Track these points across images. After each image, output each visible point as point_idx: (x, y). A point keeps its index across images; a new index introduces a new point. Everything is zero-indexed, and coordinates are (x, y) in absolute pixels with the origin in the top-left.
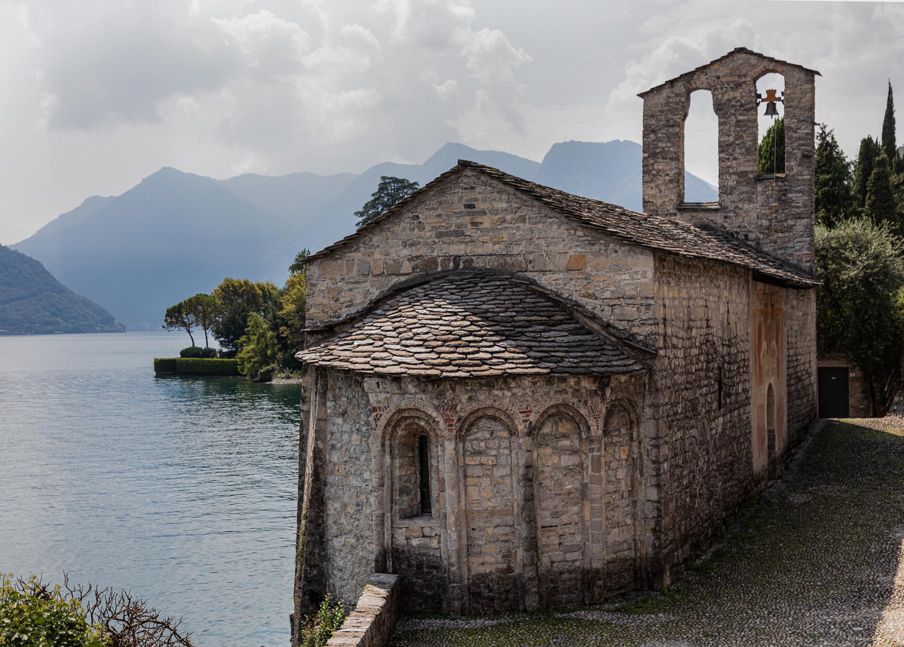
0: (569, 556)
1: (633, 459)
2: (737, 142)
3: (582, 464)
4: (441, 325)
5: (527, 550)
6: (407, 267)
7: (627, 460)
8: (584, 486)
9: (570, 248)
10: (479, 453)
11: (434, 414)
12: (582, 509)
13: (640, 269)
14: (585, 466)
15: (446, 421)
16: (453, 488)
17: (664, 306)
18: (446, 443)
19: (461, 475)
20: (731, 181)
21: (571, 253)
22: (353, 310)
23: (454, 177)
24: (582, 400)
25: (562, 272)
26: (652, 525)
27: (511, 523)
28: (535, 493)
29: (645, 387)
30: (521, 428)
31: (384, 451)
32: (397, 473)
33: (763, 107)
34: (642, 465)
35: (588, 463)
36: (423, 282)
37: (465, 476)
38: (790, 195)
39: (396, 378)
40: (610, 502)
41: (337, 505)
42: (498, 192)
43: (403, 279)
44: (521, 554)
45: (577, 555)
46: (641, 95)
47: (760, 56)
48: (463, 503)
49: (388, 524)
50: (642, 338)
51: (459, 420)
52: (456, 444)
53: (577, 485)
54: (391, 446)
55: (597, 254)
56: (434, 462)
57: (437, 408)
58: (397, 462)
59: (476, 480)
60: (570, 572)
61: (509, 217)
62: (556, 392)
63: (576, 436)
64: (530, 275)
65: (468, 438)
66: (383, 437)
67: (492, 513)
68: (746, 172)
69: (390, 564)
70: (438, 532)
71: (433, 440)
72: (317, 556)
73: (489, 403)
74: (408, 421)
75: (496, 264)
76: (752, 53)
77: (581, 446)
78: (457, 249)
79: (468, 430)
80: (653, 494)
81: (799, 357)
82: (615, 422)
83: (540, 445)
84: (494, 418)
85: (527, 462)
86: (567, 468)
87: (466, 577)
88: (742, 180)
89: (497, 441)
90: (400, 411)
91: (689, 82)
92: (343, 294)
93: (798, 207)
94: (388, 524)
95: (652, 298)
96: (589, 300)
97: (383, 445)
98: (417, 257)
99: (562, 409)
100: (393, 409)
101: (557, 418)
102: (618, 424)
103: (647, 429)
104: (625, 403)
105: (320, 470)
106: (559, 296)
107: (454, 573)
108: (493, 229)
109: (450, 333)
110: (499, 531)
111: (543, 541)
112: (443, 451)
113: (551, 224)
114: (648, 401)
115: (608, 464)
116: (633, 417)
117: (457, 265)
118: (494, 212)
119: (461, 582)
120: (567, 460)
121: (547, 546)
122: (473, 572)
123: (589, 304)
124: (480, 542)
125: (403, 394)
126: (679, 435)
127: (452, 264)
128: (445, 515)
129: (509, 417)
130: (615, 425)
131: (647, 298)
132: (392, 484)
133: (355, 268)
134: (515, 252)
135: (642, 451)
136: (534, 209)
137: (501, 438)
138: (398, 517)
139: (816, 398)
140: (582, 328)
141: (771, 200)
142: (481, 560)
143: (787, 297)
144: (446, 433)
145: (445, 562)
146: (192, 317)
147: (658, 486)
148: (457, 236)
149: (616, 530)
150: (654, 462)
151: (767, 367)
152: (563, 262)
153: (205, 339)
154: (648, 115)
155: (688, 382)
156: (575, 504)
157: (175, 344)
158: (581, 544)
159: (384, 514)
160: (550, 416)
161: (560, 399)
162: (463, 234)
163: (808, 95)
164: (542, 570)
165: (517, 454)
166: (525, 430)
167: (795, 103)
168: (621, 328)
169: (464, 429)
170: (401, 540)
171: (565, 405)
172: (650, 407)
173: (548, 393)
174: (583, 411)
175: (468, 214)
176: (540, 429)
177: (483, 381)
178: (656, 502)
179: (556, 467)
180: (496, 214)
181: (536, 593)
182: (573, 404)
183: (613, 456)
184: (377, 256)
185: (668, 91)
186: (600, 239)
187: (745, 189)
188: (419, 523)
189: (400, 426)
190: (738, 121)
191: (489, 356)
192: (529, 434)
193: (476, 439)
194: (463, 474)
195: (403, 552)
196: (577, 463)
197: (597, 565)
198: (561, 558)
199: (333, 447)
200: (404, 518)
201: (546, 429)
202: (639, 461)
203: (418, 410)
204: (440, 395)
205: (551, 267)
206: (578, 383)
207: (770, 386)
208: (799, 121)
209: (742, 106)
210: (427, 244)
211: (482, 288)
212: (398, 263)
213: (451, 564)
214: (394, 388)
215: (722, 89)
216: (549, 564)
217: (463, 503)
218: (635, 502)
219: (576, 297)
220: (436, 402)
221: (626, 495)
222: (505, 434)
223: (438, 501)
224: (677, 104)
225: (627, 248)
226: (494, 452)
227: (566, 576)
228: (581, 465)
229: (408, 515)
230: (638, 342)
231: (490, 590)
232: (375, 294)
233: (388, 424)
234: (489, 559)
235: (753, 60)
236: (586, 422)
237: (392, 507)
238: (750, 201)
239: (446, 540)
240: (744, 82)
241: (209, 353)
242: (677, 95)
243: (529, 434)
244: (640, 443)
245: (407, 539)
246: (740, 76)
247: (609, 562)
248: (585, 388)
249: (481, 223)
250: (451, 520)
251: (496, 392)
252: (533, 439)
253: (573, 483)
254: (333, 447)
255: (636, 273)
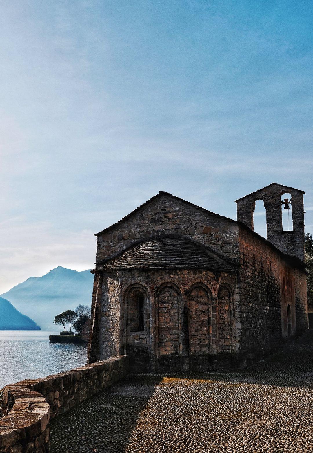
0: (203, 349)
1: (230, 310)
2: (274, 219)
3: (209, 309)
4: (150, 252)
5: (184, 345)
6: (138, 235)
7: (228, 311)
8: (209, 319)
9: (204, 225)
10: (165, 302)
11: (146, 285)
12: (208, 329)
13: (233, 231)
14: (210, 310)
15: (150, 288)
16: (153, 317)
17: (244, 248)
18: (150, 298)
19: (157, 311)
20: (272, 234)
21: (205, 226)
22: (115, 254)
23: (158, 198)
24: (209, 282)
25: (201, 234)
26: (239, 339)
27: (178, 333)
28: (188, 319)
29: (235, 280)
30: (182, 291)
31: (124, 302)
32: (130, 312)
33: (283, 206)
34: (234, 313)
35: (211, 309)
36: (146, 239)
37: (159, 312)
38: (295, 239)
39: (130, 270)
40: (220, 327)
41: (105, 329)
42: (175, 204)
43: (136, 241)
44: (181, 346)
45: (206, 349)
46: (236, 201)
47: (281, 186)
48: (157, 324)
49: (125, 333)
50: (234, 259)
51: (156, 287)
52: (155, 298)
53: (206, 318)
54: (127, 300)
55: (215, 226)
56: (145, 306)
57: (147, 283)
58: (130, 307)
59: (163, 314)
60: (203, 356)
61: (180, 213)
62: (198, 277)
63: (206, 297)
64: (188, 236)
65: (160, 296)
66: (124, 296)
67: (170, 329)
68: (278, 230)
69: (125, 351)
70: (146, 337)
71: (145, 297)
72: (95, 352)
73: (169, 280)
74: (135, 290)
75: (174, 232)
76: (278, 185)
77: (208, 302)
78: (158, 227)
79: (160, 292)
80: (239, 326)
81: (300, 300)
82: (223, 293)
83: (191, 300)
84: (171, 288)
85: (185, 306)
86: (202, 311)
87: (158, 356)
88: (276, 233)
89: (172, 298)
90: (131, 285)
91: (255, 196)
92: (112, 248)
93: (298, 244)
94: (125, 333)
95: (238, 243)
96: (212, 245)
97: (124, 300)
98: (142, 231)
99: (200, 285)
100: (128, 284)
101: (198, 289)
102: (224, 294)
103: (237, 298)
104: (227, 286)
105: (98, 315)
106: (200, 244)
107: (153, 354)
108: (173, 219)
109: (154, 254)
110: (173, 336)
111: (192, 341)
112: (149, 301)
113: (197, 215)
114: (237, 286)
115: (220, 311)
116: (231, 292)
117: (158, 233)
118: (174, 211)
119: (156, 358)
120: (202, 307)
121: (193, 343)
122: (161, 354)
123: (213, 247)
124: (164, 341)
125: (133, 277)
126: (250, 305)
127: (156, 233)
128: (149, 329)
129: (177, 287)
130: (222, 294)
131: (236, 243)
132: (127, 317)
133: (117, 237)
134: (182, 227)
135: (234, 307)
136: (190, 209)
137: (174, 296)
138: (129, 331)
139: (308, 320)
140: (209, 256)
141: (288, 241)
142: (164, 349)
143: (295, 273)
144: (150, 293)
145: (149, 350)
146: (65, 319)
147: (241, 322)
148: (158, 222)
149: (223, 340)
150: (239, 312)
151: (287, 297)
152: (202, 230)
153: (69, 327)
154: (239, 209)
155: (254, 285)
156: (205, 326)
157: (58, 329)
158: (208, 344)
159: (123, 330)
160: (195, 288)
161: (199, 280)
162: (161, 221)
163: (301, 201)
164: (191, 354)
165: (181, 303)
166: (184, 293)
167: (296, 203)
168: (225, 256)
169: (159, 292)
170: (130, 340)
171: (201, 283)
172: (237, 288)
173: (194, 278)
174: (209, 286)
175: (163, 213)
176: (191, 293)
177: (167, 271)
178: (240, 329)
179: (197, 310)
180: (174, 213)
181: (188, 363)
182: (205, 283)
183: (222, 308)
184: (126, 232)
185: (247, 199)
186: (217, 220)
187: (277, 237)
188: (139, 333)
189: (131, 292)
190: (274, 211)
191: (170, 262)
192: (186, 294)
193: (163, 296)
194: (158, 312)
195: (131, 346)
196: (206, 309)
197: (214, 353)
198: (199, 350)
199: (104, 305)
200: (133, 331)
201: (193, 293)
202: (233, 311)
203: (139, 284)
204: (148, 277)
205: (196, 232)
206: (207, 274)
207: (289, 305)
208: (298, 210)
209: (275, 205)
210: (146, 226)
211: (168, 241)
212: (134, 234)
213: (151, 350)
214: (129, 274)
215: (267, 199)
216: (194, 352)
217: (157, 324)
218: (231, 329)
219: (207, 244)
220: (147, 281)
221: (227, 325)
222: (176, 295)
223: (146, 323)
224: (250, 204)
225: (228, 223)
226: (171, 302)
227: (201, 357)
228: (208, 310)
229: (134, 330)
230: (233, 261)
231: (168, 362)
232: (124, 247)
233: (126, 291)
234: (169, 349)
235: (279, 187)
236: (211, 291)
237: (127, 327)
238: (280, 241)
239: (149, 340)
240: (276, 196)
241: (72, 333)
242: (250, 201)
243: (186, 294)
244: (233, 304)
245: (133, 340)
246: (274, 194)
247: (220, 353)
248: (210, 276)
249: (169, 216)
250: (152, 330)
251: (172, 276)
252: (188, 297)
253: (204, 317)
254: (104, 305)
255: (231, 233)
